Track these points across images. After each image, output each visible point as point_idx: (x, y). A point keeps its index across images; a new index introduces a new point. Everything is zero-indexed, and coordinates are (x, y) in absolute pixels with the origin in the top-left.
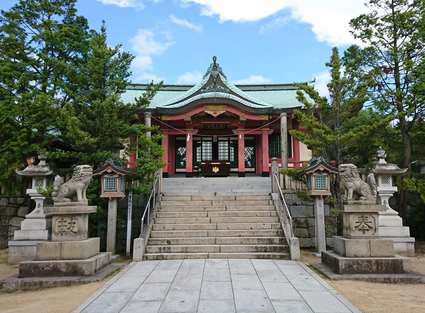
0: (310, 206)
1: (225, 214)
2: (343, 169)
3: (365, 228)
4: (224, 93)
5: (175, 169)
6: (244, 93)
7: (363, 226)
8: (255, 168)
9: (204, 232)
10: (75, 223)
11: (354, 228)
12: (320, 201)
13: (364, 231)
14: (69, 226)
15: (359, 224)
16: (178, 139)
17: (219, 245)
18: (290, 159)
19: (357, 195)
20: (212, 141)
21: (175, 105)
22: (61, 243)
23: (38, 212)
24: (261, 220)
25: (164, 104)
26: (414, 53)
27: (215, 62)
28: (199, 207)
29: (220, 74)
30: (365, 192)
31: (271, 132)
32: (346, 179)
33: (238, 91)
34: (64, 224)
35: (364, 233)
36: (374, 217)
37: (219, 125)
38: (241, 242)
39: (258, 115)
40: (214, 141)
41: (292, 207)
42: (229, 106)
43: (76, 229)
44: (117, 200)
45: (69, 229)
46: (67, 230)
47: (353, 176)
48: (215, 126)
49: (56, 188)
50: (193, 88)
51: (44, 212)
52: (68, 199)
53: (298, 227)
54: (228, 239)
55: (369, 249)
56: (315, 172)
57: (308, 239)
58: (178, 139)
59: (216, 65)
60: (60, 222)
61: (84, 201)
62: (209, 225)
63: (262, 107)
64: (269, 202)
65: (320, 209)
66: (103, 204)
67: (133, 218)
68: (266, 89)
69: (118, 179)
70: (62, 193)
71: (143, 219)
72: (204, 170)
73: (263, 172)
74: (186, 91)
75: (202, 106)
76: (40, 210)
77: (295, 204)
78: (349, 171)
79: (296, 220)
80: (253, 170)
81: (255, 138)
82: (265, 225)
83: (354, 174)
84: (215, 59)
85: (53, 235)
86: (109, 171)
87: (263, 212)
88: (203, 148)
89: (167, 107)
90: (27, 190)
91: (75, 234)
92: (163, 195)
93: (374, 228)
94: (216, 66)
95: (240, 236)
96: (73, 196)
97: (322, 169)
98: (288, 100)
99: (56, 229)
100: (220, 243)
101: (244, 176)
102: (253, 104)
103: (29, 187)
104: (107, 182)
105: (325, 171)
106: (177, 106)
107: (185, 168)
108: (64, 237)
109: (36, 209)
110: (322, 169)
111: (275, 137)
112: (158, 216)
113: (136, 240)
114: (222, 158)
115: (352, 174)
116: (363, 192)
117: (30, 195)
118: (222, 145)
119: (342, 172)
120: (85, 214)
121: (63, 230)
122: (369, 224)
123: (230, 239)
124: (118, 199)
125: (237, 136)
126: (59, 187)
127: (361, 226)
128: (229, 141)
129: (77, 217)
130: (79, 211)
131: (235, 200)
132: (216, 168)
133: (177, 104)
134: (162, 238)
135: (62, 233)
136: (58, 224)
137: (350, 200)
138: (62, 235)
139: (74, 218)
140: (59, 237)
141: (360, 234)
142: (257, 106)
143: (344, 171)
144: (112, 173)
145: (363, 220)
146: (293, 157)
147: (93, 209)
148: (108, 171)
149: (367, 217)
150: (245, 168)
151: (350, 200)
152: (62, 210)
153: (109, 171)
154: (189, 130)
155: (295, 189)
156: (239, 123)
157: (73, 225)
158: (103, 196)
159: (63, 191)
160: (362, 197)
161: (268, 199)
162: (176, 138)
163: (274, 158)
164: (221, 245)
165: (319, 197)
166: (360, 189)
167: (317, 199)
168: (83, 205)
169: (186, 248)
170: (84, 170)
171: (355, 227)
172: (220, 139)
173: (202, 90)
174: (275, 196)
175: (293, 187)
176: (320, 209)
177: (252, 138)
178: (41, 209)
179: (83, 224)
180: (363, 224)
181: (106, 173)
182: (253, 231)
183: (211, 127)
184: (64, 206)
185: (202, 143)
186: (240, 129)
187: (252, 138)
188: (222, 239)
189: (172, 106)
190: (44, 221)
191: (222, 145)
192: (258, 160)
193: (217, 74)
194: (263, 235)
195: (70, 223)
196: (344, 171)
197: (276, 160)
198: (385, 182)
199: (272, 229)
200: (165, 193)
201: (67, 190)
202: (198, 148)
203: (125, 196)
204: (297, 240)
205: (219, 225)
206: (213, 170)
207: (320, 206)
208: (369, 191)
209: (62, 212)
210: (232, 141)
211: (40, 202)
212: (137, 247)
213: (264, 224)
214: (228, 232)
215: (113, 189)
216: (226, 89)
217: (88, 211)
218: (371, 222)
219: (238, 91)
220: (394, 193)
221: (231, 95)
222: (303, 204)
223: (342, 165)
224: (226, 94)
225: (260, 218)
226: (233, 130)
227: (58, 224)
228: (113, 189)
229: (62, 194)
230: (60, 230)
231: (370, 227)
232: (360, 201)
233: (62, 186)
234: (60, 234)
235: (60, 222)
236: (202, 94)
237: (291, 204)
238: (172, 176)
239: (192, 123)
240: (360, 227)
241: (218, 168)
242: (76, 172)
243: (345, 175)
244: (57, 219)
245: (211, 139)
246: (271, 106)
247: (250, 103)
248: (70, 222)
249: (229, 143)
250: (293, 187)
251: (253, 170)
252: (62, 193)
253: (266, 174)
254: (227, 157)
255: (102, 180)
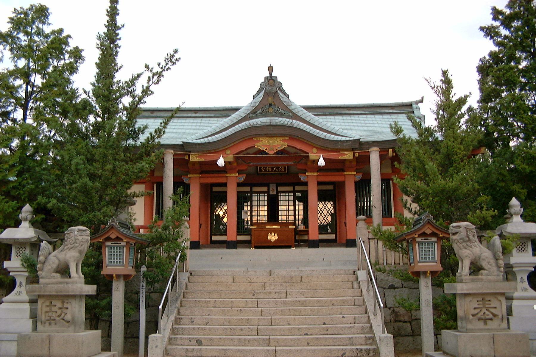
0: (414, 288)
1: (284, 302)
2: (454, 230)
3: (487, 317)
4: (284, 119)
5: (212, 235)
6: (317, 118)
7: (484, 313)
8: (335, 235)
9: (252, 329)
10: (67, 308)
11: (471, 317)
12: (426, 280)
13: (485, 321)
14: (59, 312)
15: (479, 310)
16: (215, 189)
17: (274, 348)
18: (388, 220)
19: (476, 269)
20: (268, 192)
21: (210, 138)
22: (49, 337)
23: (19, 293)
24: (340, 311)
25: (193, 137)
26: (66, 207)
27: (271, 74)
28: (244, 293)
29: (279, 91)
30: (487, 264)
31: (359, 177)
32: (461, 246)
33: (309, 116)
34: (54, 309)
35: (485, 323)
36: (500, 301)
37: (278, 168)
38: (308, 343)
39: (338, 151)
40: (271, 193)
41: (387, 292)
42: (292, 138)
43: (68, 317)
44: (124, 280)
45: (59, 316)
46: (57, 319)
47: (469, 240)
48: (272, 168)
49: (41, 258)
50: (237, 113)
51: (28, 292)
52: (58, 275)
53: (396, 321)
54: (288, 339)
55: (492, 346)
56: (419, 236)
57: (411, 338)
58: (215, 189)
59: (273, 78)
60: (47, 306)
61: (79, 277)
62: (259, 319)
63: (344, 139)
64: (352, 283)
65: (426, 292)
66: (105, 285)
67: (148, 306)
68: (351, 112)
69: (125, 249)
70: (50, 265)
71: (160, 307)
72: (252, 238)
73: (347, 240)
74: (228, 116)
75: (251, 138)
76: (21, 292)
77: (392, 287)
78: (463, 233)
79: (393, 310)
80: (333, 237)
81: (334, 187)
82: (346, 319)
83: (471, 237)
84: (271, 69)
85: (39, 324)
86: (113, 236)
87: (343, 300)
88: (254, 203)
89: (199, 141)
90: (5, 262)
91: (67, 324)
92: (191, 274)
93: (500, 316)
94: (274, 80)
95: (307, 334)
96: (64, 271)
97: (428, 232)
98: (377, 129)
99: (42, 316)
100: (276, 344)
101: (317, 246)
102: (329, 135)
103: (7, 258)
104: (110, 255)
105: (433, 234)
106: (211, 139)
107: (226, 235)
108: (53, 328)
109: (17, 289)
110: (428, 232)
111: (363, 185)
112: (183, 303)
113: (151, 336)
114: (284, 218)
115: (468, 237)
116: (484, 264)
117: (9, 270)
118: (283, 198)
119: (454, 234)
120: (81, 296)
121: (52, 318)
122: (493, 310)
123: (291, 339)
124: (126, 277)
125: (306, 184)
126: (46, 258)
127: (482, 313)
128: (294, 192)
129: (70, 300)
130: (72, 292)
131: (301, 281)
132: (273, 234)
133: (213, 137)
134: (189, 336)
135: (51, 321)
136: (45, 309)
137: (465, 276)
138: (50, 324)
139: (66, 301)
140: (47, 328)
141: (480, 325)
142: (336, 138)
143: (456, 233)
144: (118, 239)
145: (484, 304)
146: (393, 216)
147: (91, 289)
148: (111, 236)
149: (490, 301)
150: (319, 234)
151: (465, 276)
152: (52, 289)
153: (113, 236)
154: (231, 175)
155: (393, 264)
156: (309, 163)
157: (65, 311)
158: (105, 271)
159: (51, 263)
160: (482, 271)
161: (351, 279)
162: (211, 189)
163: (362, 217)
164: (278, 348)
165: (425, 273)
166: (480, 257)
167: (421, 276)
168: (79, 285)
169: (225, 350)
170: (79, 236)
171: (473, 315)
172: (280, 189)
173: (251, 115)
174: (362, 275)
175: (391, 261)
176: (426, 292)
177: (330, 187)
178: (23, 289)
179: (78, 310)
180: (484, 310)
181: (108, 239)
182: (327, 327)
183: (265, 170)
184: (53, 283)
185: (251, 196)
186: (310, 174)
187: (330, 187)
188: (278, 339)
189: (206, 140)
190: (27, 306)
191: (283, 198)
192: (340, 223)
193: (275, 90)
194: (341, 332)
195: (60, 308)
196: (456, 233)
197: (364, 220)
198: (522, 248)
199: (355, 323)
200: (193, 271)
201: (57, 262)
202: (245, 204)
203: (135, 273)
204: (390, 337)
205: (275, 319)
206: (269, 238)
207: (427, 287)
208: (493, 261)
209: (50, 292)
210: (298, 192)
211: (21, 280)
212: (154, 347)
213: (343, 317)
214: (288, 329)
215: (118, 262)
216: (287, 111)
217: (85, 292)
218: (495, 308)
219: (309, 116)
220: (534, 265)
221: (294, 121)
222: (403, 286)
223: (454, 224)
224: (288, 120)
225: (337, 308)
226: (300, 175)
227: (45, 309)
228: (118, 262)
229: (50, 268)
230: (48, 318)
231: (494, 315)
232: (480, 277)
233: (51, 257)
234: (47, 324)
235: (47, 306)
236: (250, 121)
237: (387, 286)
238: (205, 247)
239: (235, 164)
240: (479, 315)
241: (276, 235)
242: (68, 236)
243: (458, 238)
244: (44, 302)
245: (265, 189)
246: (357, 137)
247: (325, 134)
248: (61, 306)
249: (294, 195)
250: (391, 261)
251: (333, 237)
252: (50, 265)
253: (352, 243)
254: (292, 218)
255: (103, 251)
